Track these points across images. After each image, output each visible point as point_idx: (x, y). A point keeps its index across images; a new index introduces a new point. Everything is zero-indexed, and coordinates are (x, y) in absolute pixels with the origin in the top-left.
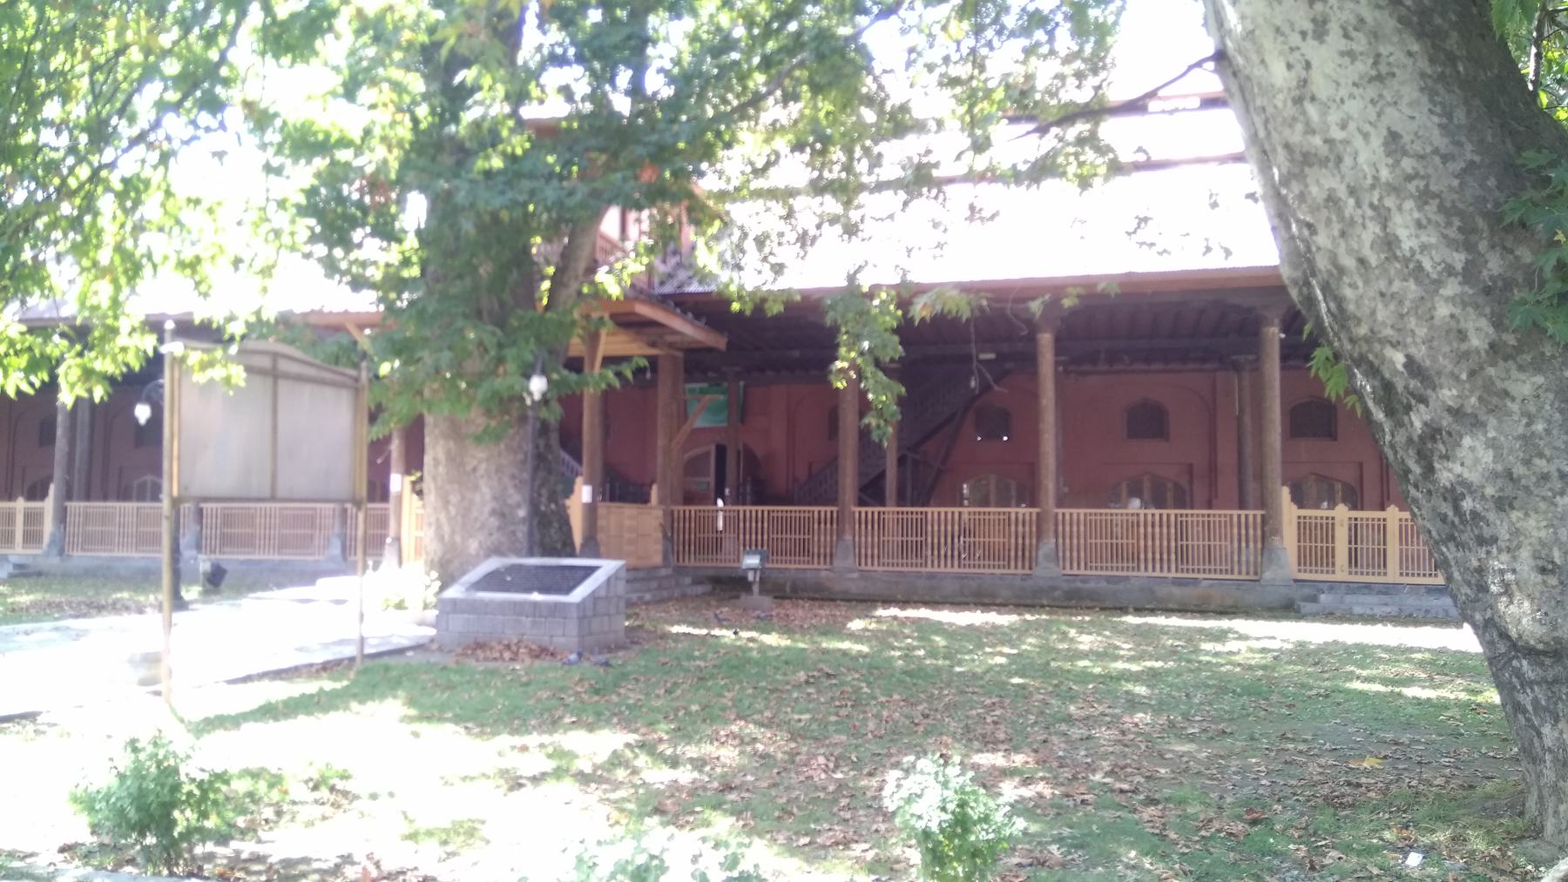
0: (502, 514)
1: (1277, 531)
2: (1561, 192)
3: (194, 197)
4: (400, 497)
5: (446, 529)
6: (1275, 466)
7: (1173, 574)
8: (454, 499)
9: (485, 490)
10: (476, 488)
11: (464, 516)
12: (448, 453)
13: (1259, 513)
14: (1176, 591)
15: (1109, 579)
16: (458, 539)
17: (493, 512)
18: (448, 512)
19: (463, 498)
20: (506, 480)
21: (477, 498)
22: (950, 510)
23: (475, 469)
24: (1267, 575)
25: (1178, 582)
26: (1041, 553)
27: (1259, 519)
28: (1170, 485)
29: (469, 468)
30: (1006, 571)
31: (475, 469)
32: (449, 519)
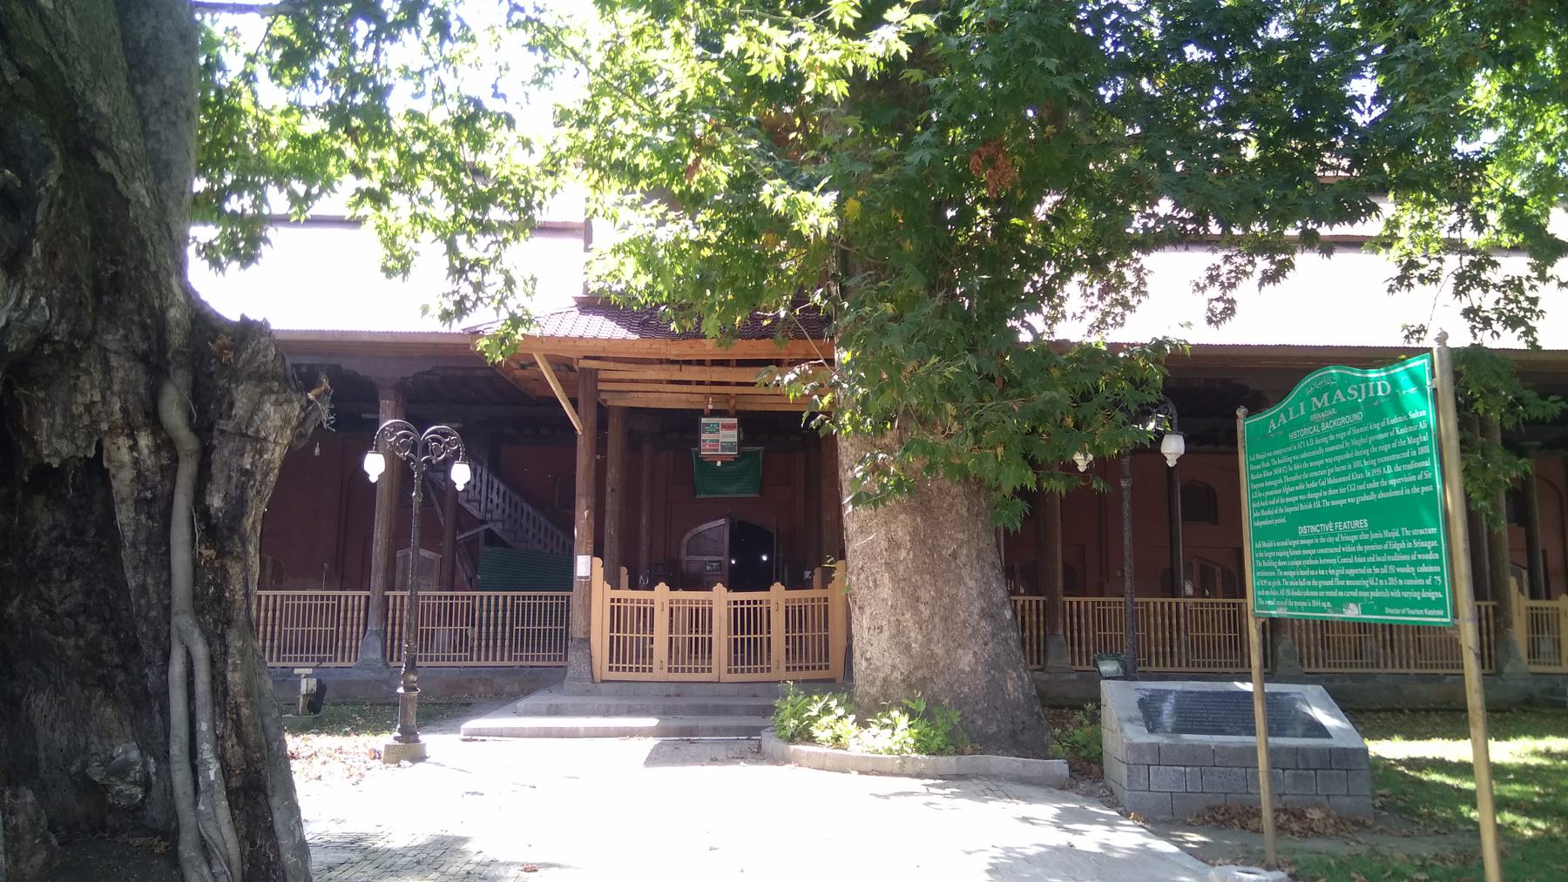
0: (989, 615)
1: (1509, 624)
2: (534, 279)
3: (1183, 322)
4: (588, 582)
5: (915, 636)
6: (1507, 565)
7: (1413, 671)
8: (926, 594)
9: (971, 583)
10: (960, 580)
11: (945, 620)
12: (914, 534)
13: (1490, 603)
14: (1422, 688)
15: (1352, 676)
16: (939, 650)
17: (984, 614)
18: (917, 612)
19: (940, 594)
20: (987, 569)
21: (962, 595)
22: (1082, 599)
23: (954, 555)
24: (1507, 669)
25: (1422, 678)
26: (1280, 649)
27: (1491, 611)
28: (1218, 570)
29: (946, 553)
30: (468, 663)
31: (954, 555)
32: (920, 623)
